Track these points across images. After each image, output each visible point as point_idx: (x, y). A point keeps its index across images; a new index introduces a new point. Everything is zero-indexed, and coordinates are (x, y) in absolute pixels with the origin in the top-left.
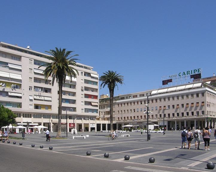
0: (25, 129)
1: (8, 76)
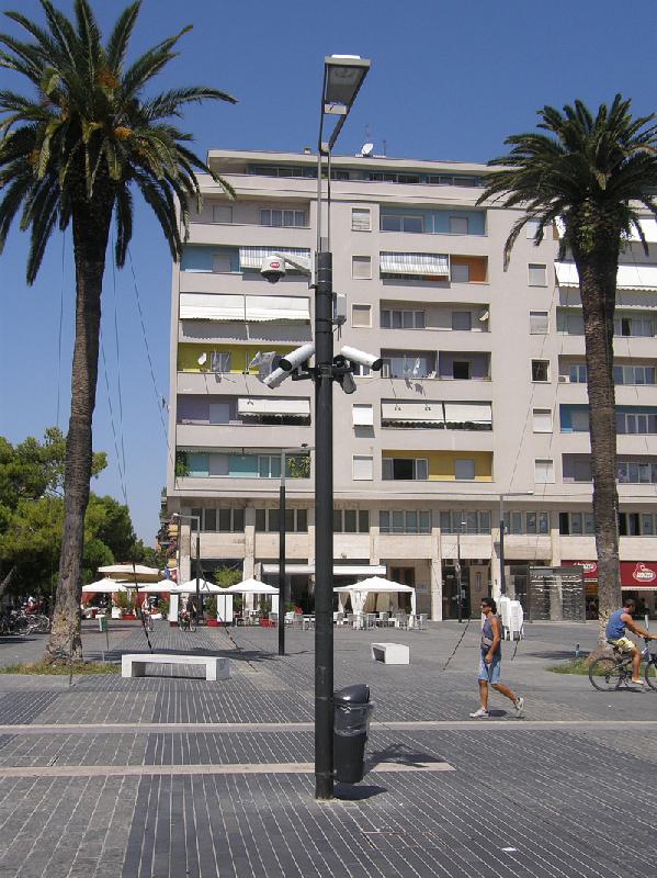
0: (411, 593)
1: (237, 314)
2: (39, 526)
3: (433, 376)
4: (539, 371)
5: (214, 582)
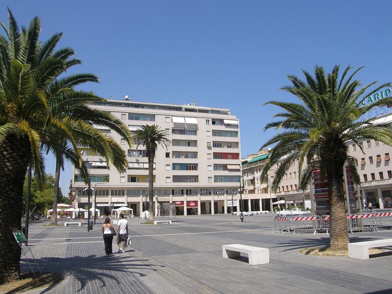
2: (42, 197)
3: (141, 156)
4: (167, 155)
5: (83, 208)
